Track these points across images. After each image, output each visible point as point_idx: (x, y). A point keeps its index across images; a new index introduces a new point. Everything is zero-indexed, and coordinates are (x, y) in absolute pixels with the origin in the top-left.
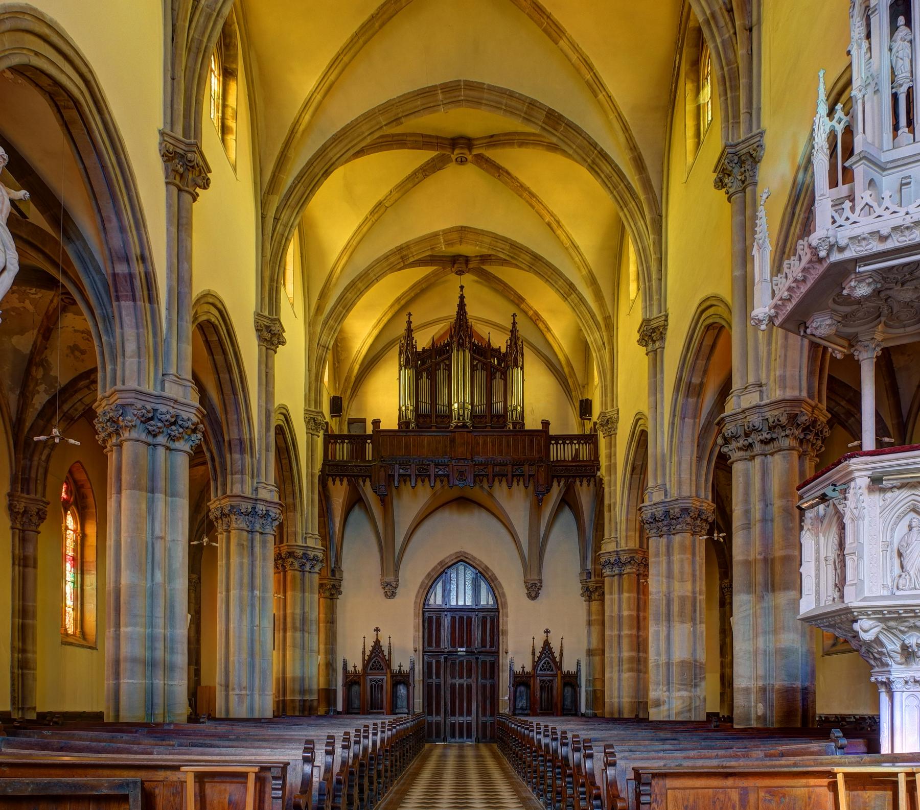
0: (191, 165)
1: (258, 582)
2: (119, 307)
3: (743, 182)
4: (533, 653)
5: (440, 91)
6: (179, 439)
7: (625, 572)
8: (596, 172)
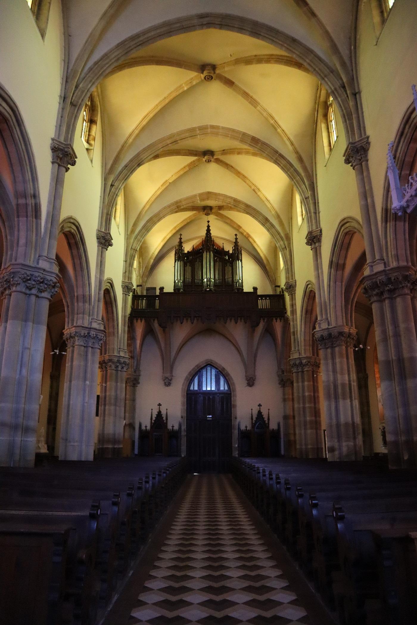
0: (66, 153)
1: (89, 375)
2: (18, 221)
3: (360, 160)
4: (252, 419)
5: (198, 129)
6: (44, 291)
7: (305, 370)
8: (278, 163)
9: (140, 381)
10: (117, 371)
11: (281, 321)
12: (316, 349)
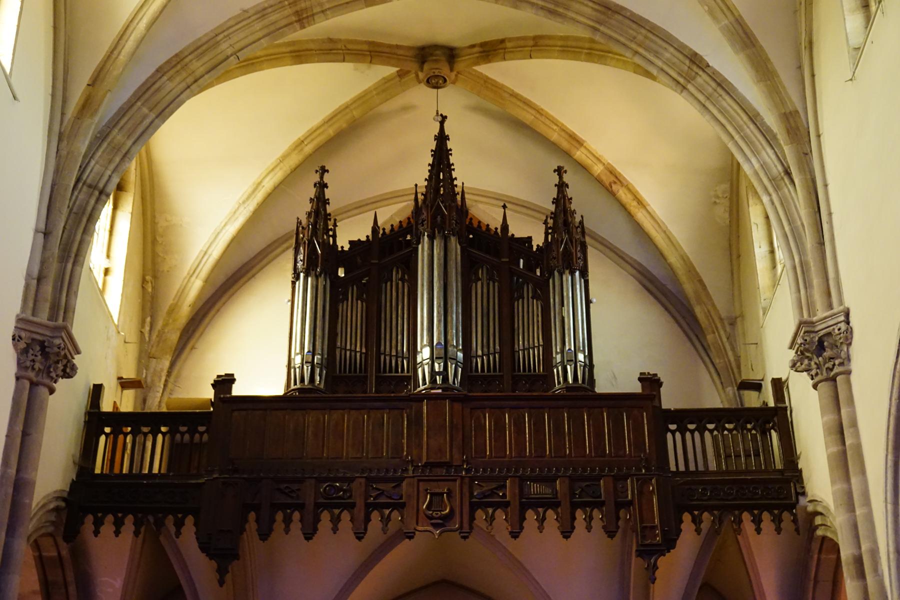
11: (779, 530)
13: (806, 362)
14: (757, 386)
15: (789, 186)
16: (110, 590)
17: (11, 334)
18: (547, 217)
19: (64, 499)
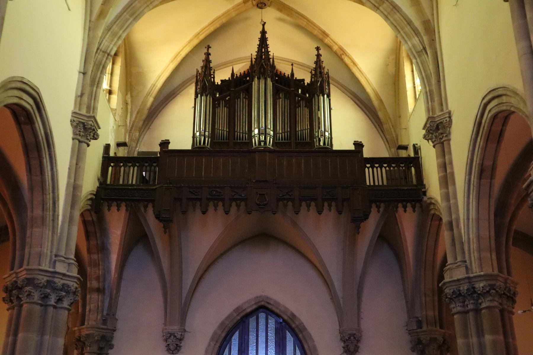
7: (484, 305)
9: (114, 342)
10: (45, 306)
11: (414, 211)
12: (504, 260)
13: (430, 135)
14: (405, 148)
15: (425, 55)
16: (115, 236)
17: (70, 119)
18: (312, 70)
19: (94, 195)
